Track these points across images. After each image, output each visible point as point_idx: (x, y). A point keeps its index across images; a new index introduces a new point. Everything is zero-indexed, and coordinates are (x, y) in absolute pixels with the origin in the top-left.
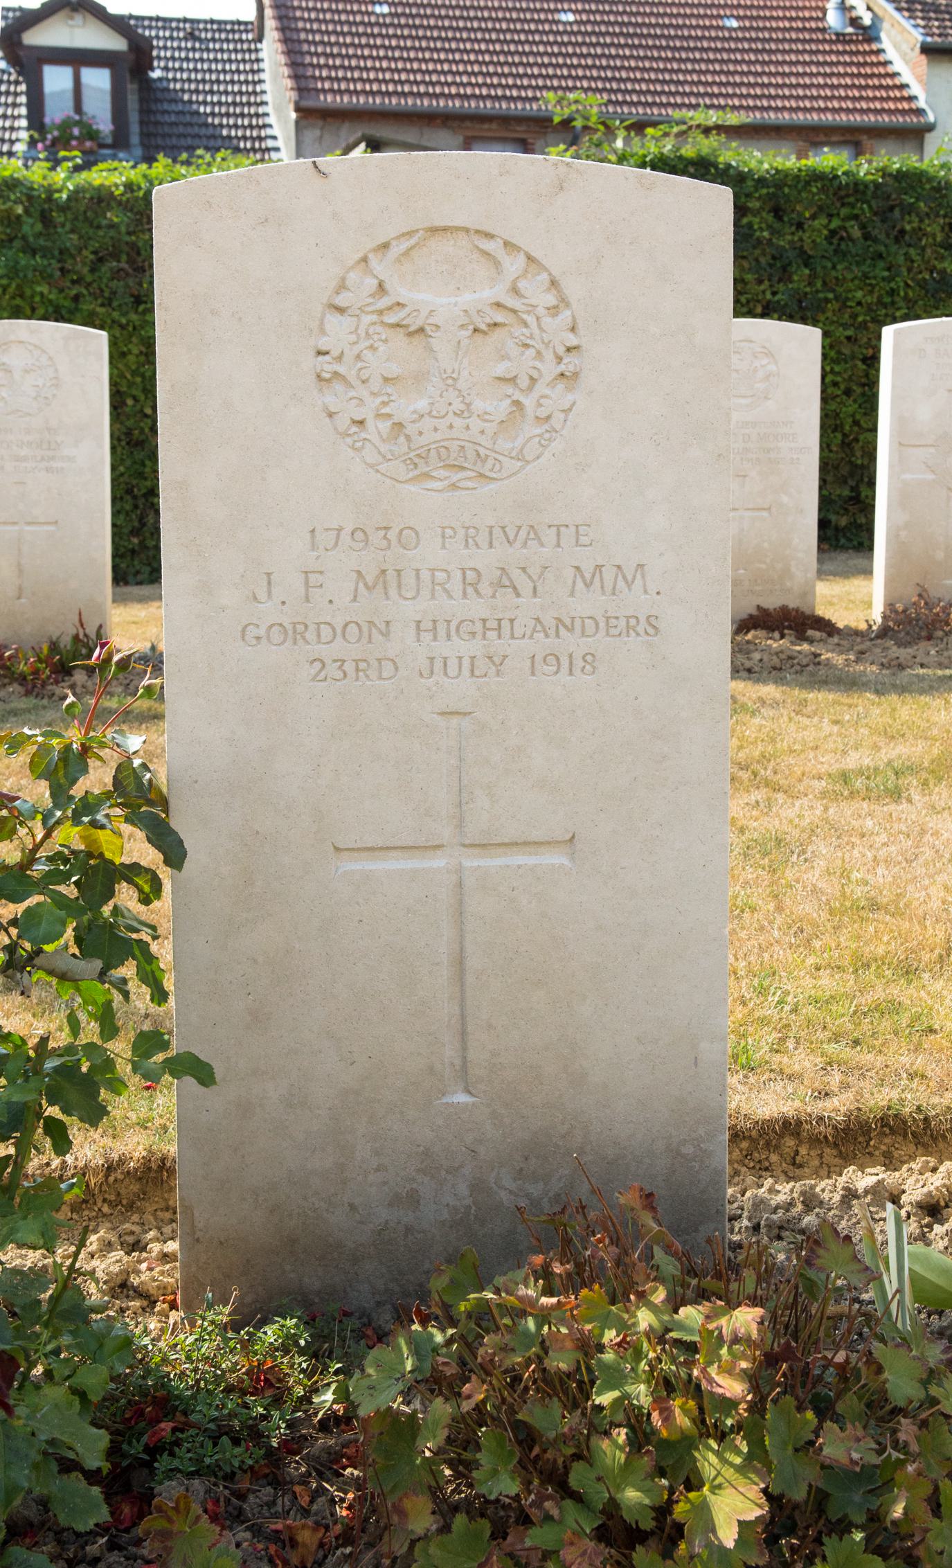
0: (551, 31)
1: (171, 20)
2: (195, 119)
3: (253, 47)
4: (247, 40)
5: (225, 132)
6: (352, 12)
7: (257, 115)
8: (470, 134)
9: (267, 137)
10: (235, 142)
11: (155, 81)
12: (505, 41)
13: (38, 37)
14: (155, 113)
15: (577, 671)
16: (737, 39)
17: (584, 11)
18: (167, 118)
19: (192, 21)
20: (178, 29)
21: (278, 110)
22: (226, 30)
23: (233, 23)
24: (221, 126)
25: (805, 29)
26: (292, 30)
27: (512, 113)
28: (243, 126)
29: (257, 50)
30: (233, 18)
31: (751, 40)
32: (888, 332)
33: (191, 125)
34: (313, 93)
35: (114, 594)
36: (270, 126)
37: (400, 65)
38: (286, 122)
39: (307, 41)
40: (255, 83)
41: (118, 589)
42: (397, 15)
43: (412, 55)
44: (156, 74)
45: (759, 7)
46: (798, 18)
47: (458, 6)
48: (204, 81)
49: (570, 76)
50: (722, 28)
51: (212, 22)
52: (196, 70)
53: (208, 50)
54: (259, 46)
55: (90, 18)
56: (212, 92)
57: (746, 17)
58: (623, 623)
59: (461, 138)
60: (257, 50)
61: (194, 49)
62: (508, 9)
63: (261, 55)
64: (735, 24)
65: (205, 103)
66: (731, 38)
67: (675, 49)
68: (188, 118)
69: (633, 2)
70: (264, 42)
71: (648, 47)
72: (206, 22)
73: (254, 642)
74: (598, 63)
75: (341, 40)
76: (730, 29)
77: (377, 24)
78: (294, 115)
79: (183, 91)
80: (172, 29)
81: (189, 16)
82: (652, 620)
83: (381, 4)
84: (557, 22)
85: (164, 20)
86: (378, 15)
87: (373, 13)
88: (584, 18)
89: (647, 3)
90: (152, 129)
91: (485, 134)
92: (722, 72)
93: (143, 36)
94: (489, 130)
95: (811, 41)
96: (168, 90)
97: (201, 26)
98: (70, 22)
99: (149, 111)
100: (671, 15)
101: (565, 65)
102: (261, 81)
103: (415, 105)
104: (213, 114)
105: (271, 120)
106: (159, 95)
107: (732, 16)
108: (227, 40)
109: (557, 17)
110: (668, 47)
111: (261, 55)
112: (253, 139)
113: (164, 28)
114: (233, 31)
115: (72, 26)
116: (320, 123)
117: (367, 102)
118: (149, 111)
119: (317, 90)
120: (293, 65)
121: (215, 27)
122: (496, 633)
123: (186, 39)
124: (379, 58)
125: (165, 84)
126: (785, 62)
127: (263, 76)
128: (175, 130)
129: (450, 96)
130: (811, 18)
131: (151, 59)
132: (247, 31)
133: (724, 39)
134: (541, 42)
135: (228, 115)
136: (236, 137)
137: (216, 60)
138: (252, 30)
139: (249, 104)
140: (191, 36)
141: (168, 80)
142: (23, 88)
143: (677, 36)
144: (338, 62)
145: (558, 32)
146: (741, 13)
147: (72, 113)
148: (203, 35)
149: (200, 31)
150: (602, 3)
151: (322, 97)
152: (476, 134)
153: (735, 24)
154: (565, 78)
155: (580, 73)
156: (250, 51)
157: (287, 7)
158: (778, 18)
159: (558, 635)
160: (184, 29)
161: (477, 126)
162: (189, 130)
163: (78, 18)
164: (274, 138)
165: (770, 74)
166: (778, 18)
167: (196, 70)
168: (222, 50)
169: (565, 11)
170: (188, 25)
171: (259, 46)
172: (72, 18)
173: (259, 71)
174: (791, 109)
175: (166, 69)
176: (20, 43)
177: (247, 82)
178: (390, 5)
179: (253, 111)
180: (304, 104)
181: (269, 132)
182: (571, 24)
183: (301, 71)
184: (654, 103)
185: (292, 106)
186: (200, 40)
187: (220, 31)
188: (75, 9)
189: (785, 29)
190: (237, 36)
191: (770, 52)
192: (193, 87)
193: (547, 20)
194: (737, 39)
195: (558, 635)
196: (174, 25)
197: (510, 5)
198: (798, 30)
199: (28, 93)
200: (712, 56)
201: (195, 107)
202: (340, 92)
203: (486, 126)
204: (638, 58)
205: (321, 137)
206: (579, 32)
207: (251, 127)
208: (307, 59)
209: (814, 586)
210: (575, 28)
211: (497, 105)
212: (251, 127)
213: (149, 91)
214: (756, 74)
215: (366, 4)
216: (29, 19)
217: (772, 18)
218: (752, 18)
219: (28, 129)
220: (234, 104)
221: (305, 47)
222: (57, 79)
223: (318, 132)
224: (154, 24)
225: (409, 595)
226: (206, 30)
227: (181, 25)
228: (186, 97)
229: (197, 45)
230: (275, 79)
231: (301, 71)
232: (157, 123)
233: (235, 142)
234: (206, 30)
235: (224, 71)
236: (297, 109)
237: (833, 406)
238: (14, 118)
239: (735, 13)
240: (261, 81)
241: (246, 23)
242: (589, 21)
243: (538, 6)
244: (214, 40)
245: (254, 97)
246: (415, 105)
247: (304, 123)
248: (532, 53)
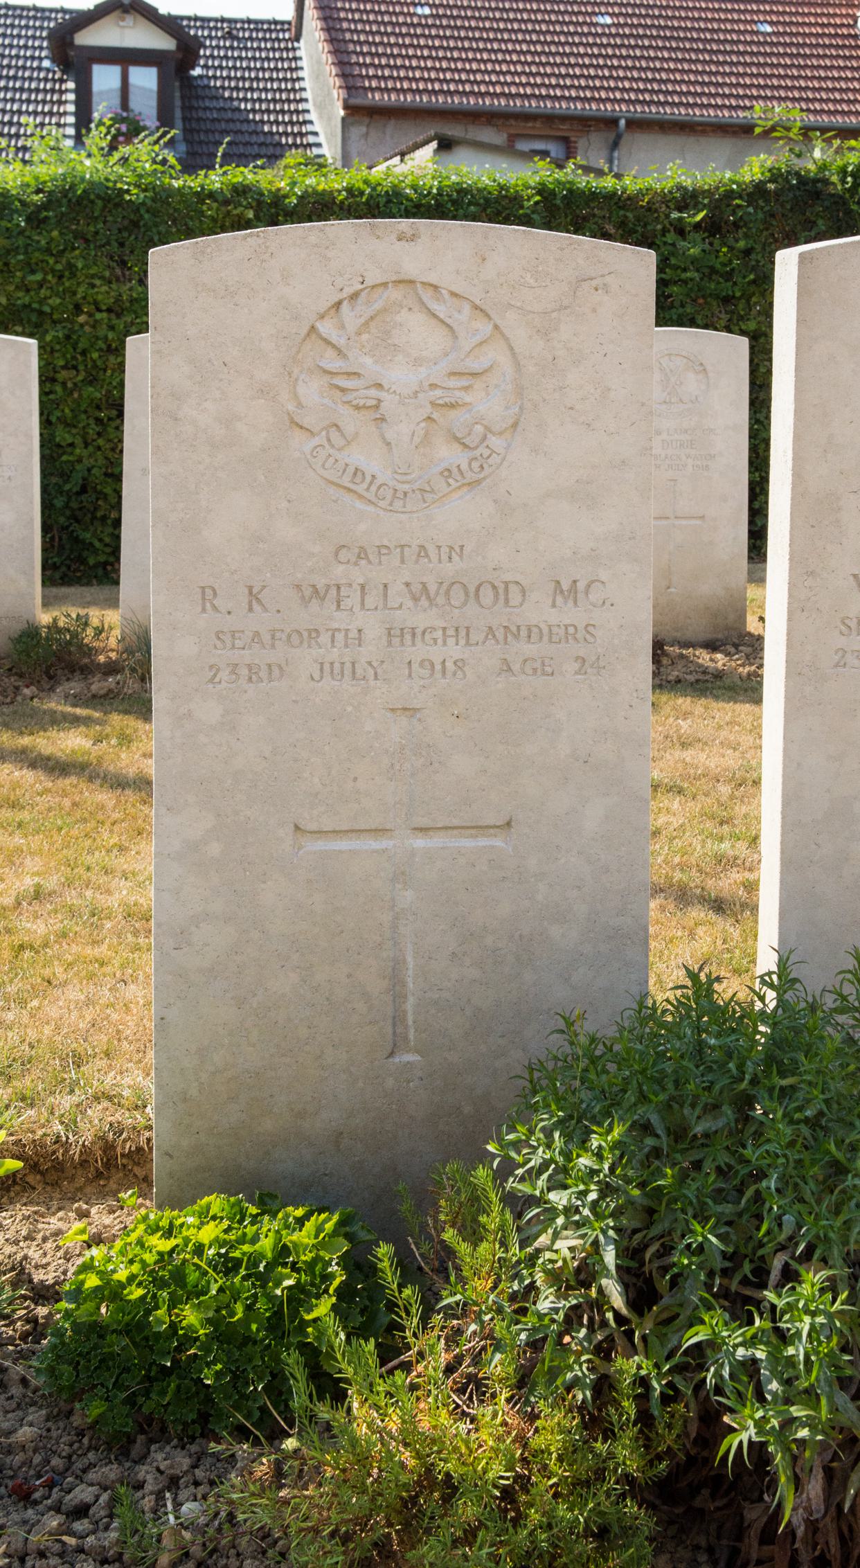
0: (590, 33)
1: (209, 20)
2: (236, 116)
3: (290, 46)
4: (284, 39)
5: (266, 129)
6: (380, 12)
7: (297, 112)
8: (512, 132)
9: (307, 133)
10: (277, 137)
11: (196, 78)
12: (430, 36)
13: (89, 38)
15: (449, 674)
16: (772, 44)
17: (621, 14)
19: (230, 21)
20: (216, 29)
21: (320, 107)
22: (262, 29)
23: (269, 22)
24: (262, 122)
25: (837, 35)
26: (337, 30)
27: (586, 113)
28: (283, 122)
29: (294, 49)
30: (269, 17)
31: (785, 45)
33: (233, 121)
34: (361, 91)
35: (44, 597)
36: (311, 122)
37: (429, 64)
38: (329, 119)
39: (352, 41)
40: (294, 80)
41: (47, 591)
42: (438, 16)
43: (411, 52)
44: (197, 72)
45: (662, 7)
46: (830, 24)
47: (455, 6)
48: (243, 79)
49: (611, 77)
50: (757, 33)
51: (249, 21)
52: (235, 68)
53: (246, 49)
54: (296, 44)
55: (141, 19)
56: (251, 89)
57: (779, 22)
58: (562, 631)
59: (505, 135)
60: (294, 49)
61: (232, 48)
62: (477, 8)
63: (298, 54)
64: (769, 29)
65: (245, 100)
66: (766, 43)
67: (711, 52)
68: (230, 115)
69: (589, 3)
70: (302, 41)
71: (685, 49)
72: (243, 22)
73: (531, 672)
74: (638, 65)
75: (386, 40)
76: (765, 34)
77: (420, 24)
78: (342, 113)
79: (223, 88)
80: (211, 29)
81: (226, 15)
82: (590, 629)
83: (422, 5)
84: (596, 25)
85: (203, 19)
86: (419, 16)
87: (415, 14)
88: (622, 21)
89: (602, 3)
90: (194, 125)
91: (532, 133)
92: (759, 75)
93: (196, 36)
94: (533, 128)
95: (844, 46)
96: (209, 87)
97: (239, 26)
98: (121, 24)
99: (191, 108)
100: (706, 20)
101: (606, 66)
102: (299, 79)
103: (492, 105)
104: (254, 111)
105: (312, 116)
106: (200, 92)
107: (766, 21)
108: (265, 40)
109: (595, 20)
110: (705, 50)
111: (298, 54)
112: (295, 135)
113: (203, 28)
114: (270, 31)
115: (123, 27)
116: (366, 120)
117: (530, 105)
118: (191, 108)
119: (364, 88)
120: (340, 64)
121: (198, 24)
122: (398, 639)
123: (223, 37)
125: (206, 81)
126: (820, 67)
127: (301, 74)
128: (217, 126)
129: (495, 95)
130: (843, 25)
131: (198, 57)
132: (284, 31)
133: (759, 43)
134: (524, 41)
135: (268, 111)
136: (278, 132)
137: (254, 58)
138: (289, 30)
139: (289, 101)
140: (230, 35)
141: (209, 78)
142: (71, 85)
143: (713, 40)
144: (383, 61)
145: (597, 35)
146: (616, 10)
147: (119, 111)
148: (241, 35)
149: (238, 30)
150: (557, 3)
151: (370, 95)
152: (520, 132)
153: (769, 29)
154: (607, 78)
155: (534, 69)
156: (287, 49)
157: (331, 9)
158: (810, 25)
159: (506, 643)
160: (223, 28)
161: (523, 124)
162: (231, 126)
163: (129, 20)
164: (316, 134)
165: (806, 78)
166: (810, 25)
167: (263, 69)
168: (260, 49)
169: (602, 15)
170: (60, 16)
171: (296, 44)
172: (123, 20)
173: (297, 69)
174: (829, 112)
175: (206, 67)
176: (72, 43)
177: (285, 79)
178: (430, 6)
179: (292, 107)
180: (353, 101)
181: (309, 128)
182: (609, 26)
183: (348, 70)
184: (696, 104)
185: (340, 104)
186: (238, 39)
187: (257, 30)
188: (126, 10)
189: (817, 35)
190: (274, 36)
191: (805, 56)
192: (233, 84)
193: (585, 23)
194: (772, 44)
195: (506, 643)
196: (212, 24)
197: (493, 5)
198: (830, 36)
199: (76, 91)
200: (748, 60)
201: (236, 103)
202: (387, 90)
203: (530, 124)
204: (677, 60)
205: (367, 133)
206: (617, 35)
207: (292, 123)
208: (354, 59)
209: (746, 588)
210: (613, 31)
211: (542, 104)
212: (292, 123)
213: (188, 84)
214: (793, 77)
215: (379, 3)
216: (85, 19)
217: (805, 24)
218: (784, 24)
220: (274, 101)
221: (351, 47)
222: (105, 78)
223: (364, 129)
224: (192, 23)
225: (457, 604)
226: (244, 29)
227: (219, 25)
228: (227, 94)
229: (235, 44)
230: (317, 76)
231: (348, 70)
232: (199, 120)
233: (277, 137)
234: (244, 29)
235: (263, 69)
236: (346, 107)
237: (112, 360)
238: (60, 115)
239: (768, 18)
240: (299, 79)
241: (282, 23)
242: (626, 24)
243: (521, 6)
244: (251, 38)
245: (294, 94)
246: (492, 105)
247: (351, 120)
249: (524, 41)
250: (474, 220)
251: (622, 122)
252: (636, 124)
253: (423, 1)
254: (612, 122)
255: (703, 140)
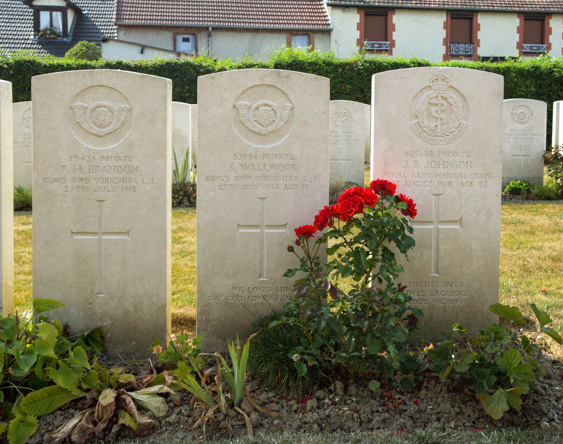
8: (175, 32)
14: (81, 25)
18: (84, 27)
32: (10, 84)
47: (226, 2)
62: (247, 3)
68: (91, 27)
116: (125, 29)
119: (123, 19)
124: (263, 11)
141: (88, 14)
219: (34, 31)
223: (124, 32)
243: (286, 3)
247: (120, 29)
248: (317, 12)
249: (312, 8)
250: (23, 101)
251: (210, 28)
252: (215, 29)
253: (220, 1)
254: (207, 28)
255: (241, 34)
